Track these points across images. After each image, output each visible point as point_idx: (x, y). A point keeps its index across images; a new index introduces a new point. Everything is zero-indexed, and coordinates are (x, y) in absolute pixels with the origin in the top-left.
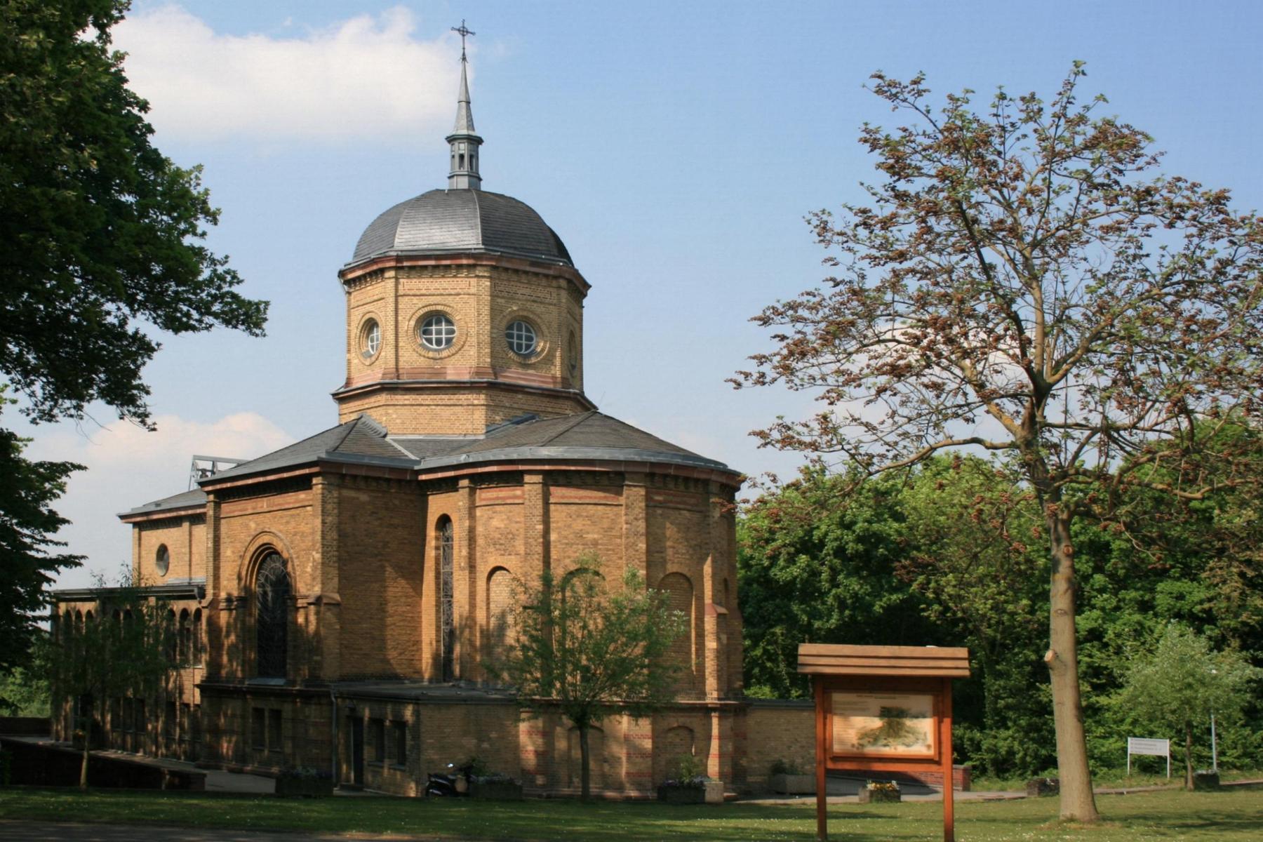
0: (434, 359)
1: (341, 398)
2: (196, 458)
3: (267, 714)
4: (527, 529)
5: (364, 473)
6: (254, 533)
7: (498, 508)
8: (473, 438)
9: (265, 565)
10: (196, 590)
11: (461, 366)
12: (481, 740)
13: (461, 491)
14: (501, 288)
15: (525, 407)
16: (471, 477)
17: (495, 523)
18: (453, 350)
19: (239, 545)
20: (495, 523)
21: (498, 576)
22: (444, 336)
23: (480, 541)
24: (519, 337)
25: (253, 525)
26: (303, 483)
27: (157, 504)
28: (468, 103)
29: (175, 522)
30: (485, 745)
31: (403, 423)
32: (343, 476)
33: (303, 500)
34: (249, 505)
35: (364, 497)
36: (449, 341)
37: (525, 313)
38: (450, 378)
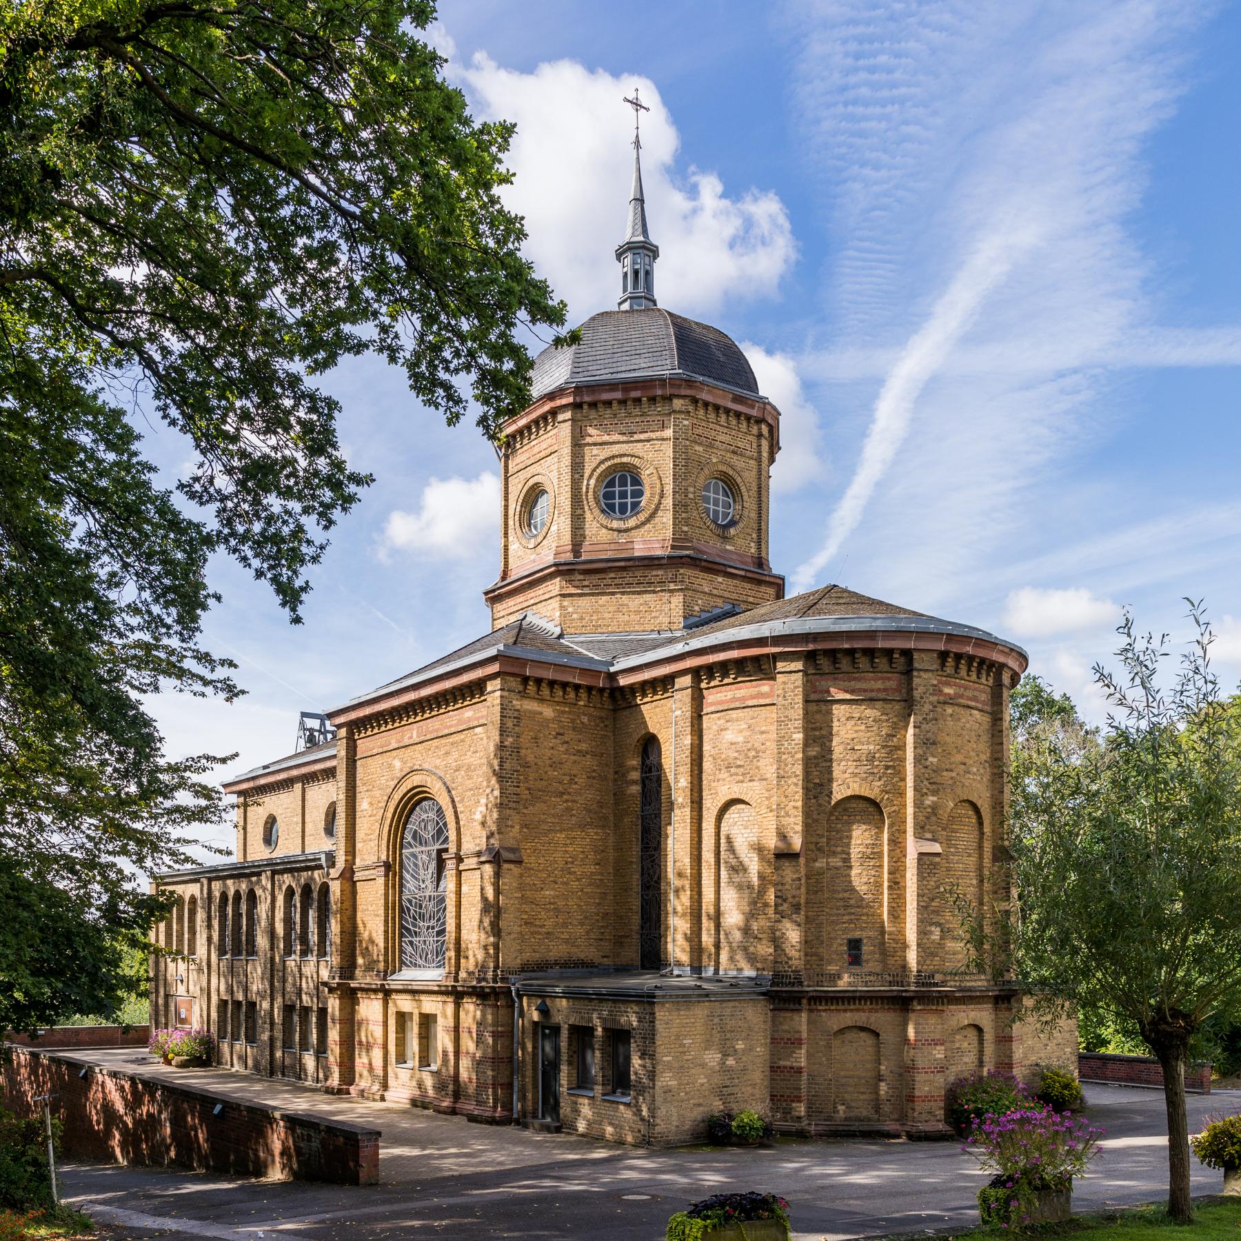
0: (619, 531)
1: (494, 597)
2: (304, 715)
3: (564, 1034)
4: (779, 742)
5: (550, 675)
6: (399, 775)
7: (734, 714)
8: (669, 635)
9: (413, 818)
10: (323, 857)
11: (654, 537)
12: (725, 1055)
13: (678, 695)
14: (700, 431)
15: (726, 595)
16: (696, 672)
17: (729, 736)
18: (642, 517)
19: (377, 793)
20: (729, 736)
21: (733, 814)
22: (629, 500)
23: (707, 765)
24: (716, 503)
25: (397, 764)
26: (475, 689)
27: (265, 767)
28: (642, 201)
29: (287, 784)
30: (731, 1062)
31: (582, 619)
32: (526, 680)
33: (469, 719)
34: (391, 737)
35: (548, 712)
36: (635, 505)
37: (724, 468)
38: (637, 554)
